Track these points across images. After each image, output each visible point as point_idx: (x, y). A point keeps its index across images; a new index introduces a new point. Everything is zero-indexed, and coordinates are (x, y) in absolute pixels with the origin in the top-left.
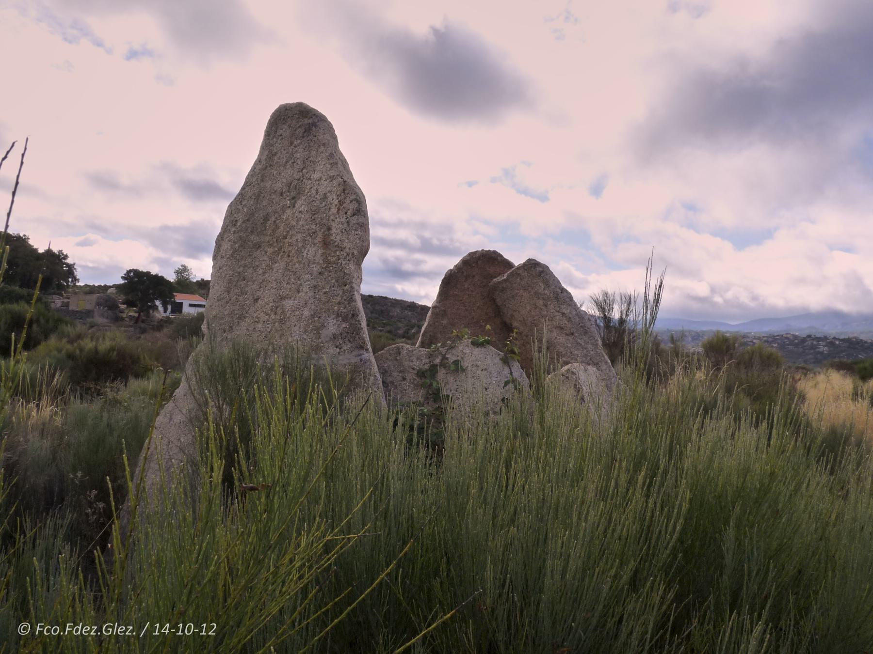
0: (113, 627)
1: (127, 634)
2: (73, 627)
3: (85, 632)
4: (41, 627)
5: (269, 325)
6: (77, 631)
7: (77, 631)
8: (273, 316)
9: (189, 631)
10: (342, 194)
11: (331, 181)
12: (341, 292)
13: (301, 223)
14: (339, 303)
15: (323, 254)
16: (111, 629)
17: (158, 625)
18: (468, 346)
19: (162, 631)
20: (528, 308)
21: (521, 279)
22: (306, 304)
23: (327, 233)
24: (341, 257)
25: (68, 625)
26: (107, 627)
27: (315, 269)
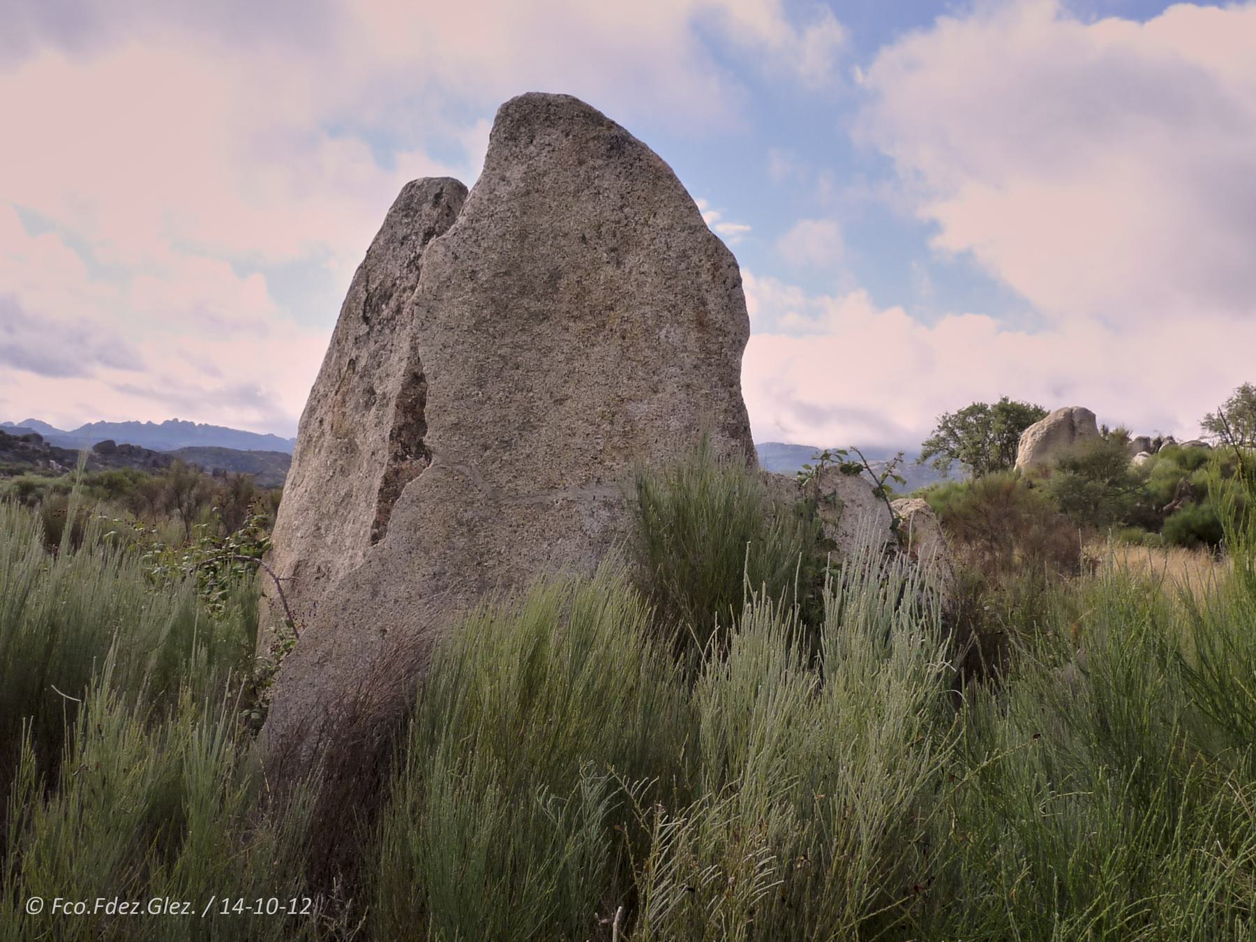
1: (132, 913)
2: (104, 903)
3: (123, 910)
4: (100, 903)
5: (599, 441)
6: (110, 910)
7: (110, 910)
8: (606, 426)
9: (271, 910)
10: (715, 254)
11: (693, 233)
12: (726, 395)
13: (647, 289)
14: (726, 411)
15: (698, 339)
16: (160, 907)
17: (227, 900)
18: (837, 474)
19: (233, 909)
22: (673, 410)
23: (702, 308)
24: (725, 344)
25: (98, 899)
27: (688, 361)
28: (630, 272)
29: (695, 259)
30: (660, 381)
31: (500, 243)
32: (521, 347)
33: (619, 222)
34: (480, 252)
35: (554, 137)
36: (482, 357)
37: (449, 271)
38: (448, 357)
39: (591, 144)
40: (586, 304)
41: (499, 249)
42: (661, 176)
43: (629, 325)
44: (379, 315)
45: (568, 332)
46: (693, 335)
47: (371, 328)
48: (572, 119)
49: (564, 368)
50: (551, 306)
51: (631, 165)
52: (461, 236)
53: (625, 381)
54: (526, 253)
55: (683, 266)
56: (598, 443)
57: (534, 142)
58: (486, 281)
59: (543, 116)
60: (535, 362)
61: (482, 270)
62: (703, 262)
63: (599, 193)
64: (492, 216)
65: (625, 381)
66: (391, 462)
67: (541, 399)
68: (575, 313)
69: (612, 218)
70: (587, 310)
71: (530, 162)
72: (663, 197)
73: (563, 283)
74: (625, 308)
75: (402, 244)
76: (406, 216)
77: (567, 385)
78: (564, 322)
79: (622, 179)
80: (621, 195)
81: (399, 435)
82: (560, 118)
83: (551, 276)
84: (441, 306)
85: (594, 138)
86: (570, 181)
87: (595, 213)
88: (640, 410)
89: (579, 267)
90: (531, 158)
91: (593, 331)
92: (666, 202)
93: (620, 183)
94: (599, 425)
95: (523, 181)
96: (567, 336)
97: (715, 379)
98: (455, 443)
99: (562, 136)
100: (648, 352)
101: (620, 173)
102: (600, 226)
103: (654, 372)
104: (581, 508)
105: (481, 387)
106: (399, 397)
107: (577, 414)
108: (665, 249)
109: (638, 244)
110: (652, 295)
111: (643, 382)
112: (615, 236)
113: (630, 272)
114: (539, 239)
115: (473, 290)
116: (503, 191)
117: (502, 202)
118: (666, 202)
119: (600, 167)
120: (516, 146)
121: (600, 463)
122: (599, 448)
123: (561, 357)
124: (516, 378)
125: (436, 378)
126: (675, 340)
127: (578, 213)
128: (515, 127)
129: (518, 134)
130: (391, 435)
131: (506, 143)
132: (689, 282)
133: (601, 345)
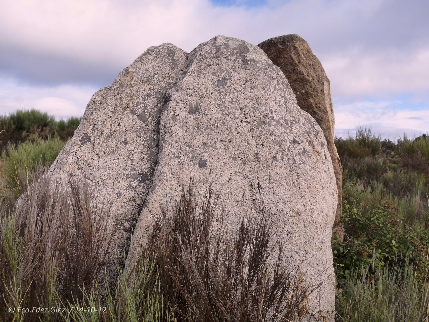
16: (54, 310)
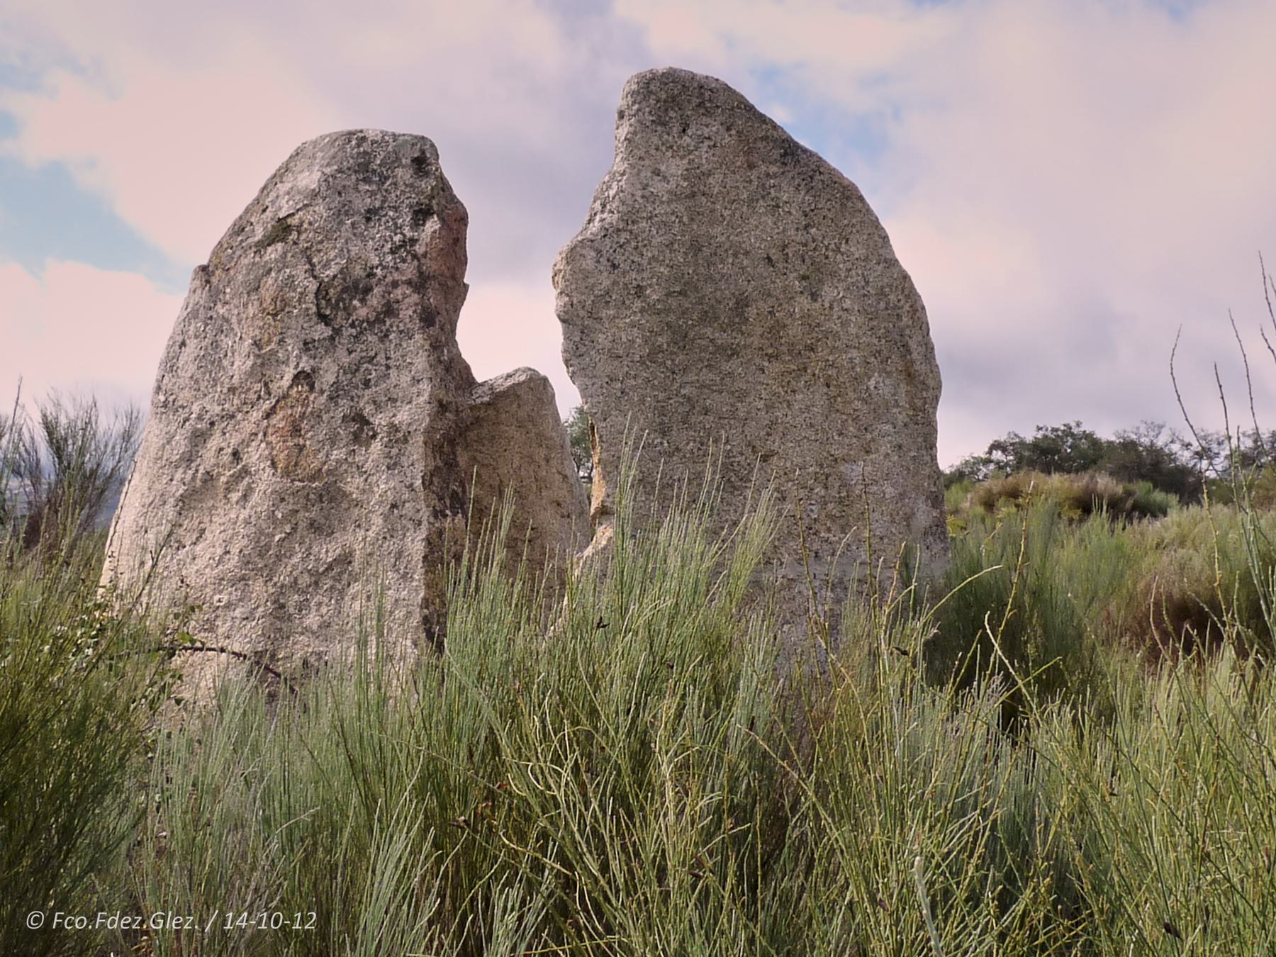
0: (164, 918)
2: (106, 918)
4: (59, 917)
5: (813, 508)
8: (819, 490)
20: (516, 463)
21: (519, 406)
26: (154, 922)
28: (831, 308)
29: (892, 297)
30: (873, 440)
31: (668, 255)
32: (708, 387)
33: (805, 245)
34: (645, 262)
35: (714, 129)
36: (661, 396)
37: (607, 283)
38: (619, 394)
39: (759, 144)
40: (783, 341)
41: (667, 262)
42: (848, 196)
43: (835, 371)
44: (350, 315)
45: (764, 372)
46: (903, 388)
47: (337, 332)
48: (733, 109)
49: (765, 418)
50: (740, 339)
51: (811, 178)
52: (616, 239)
53: (836, 438)
54: (702, 270)
55: (882, 305)
56: (812, 511)
57: (689, 132)
58: (658, 300)
59: (695, 101)
60: (729, 408)
61: (650, 285)
62: (902, 302)
63: (778, 207)
64: (650, 218)
65: (836, 438)
66: (432, 520)
67: (742, 454)
68: (770, 351)
69: (798, 239)
70: (784, 349)
71: (691, 157)
72: (854, 221)
73: (752, 312)
74: (828, 350)
75: (368, 220)
76: (365, 180)
77: (771, 438)
78: (758, 361)
79: (803, 193)
80: (804, 212)
81: (431, 482)
82: (718, 107)
83: (737, 303)
84: (598, 326)
85: (762, 139)
86: (741, 187)
87: (776, 231)
88: (854, 472)
89: (769, 295)
90: (690, 152)
91: (793, 375)
92: (858, 227)
93: (801, 196)
94: (812, 489)
95: (685, 180)
96: (762, 378)
97: (920, 440)
98: (642, 504)
99: (722, 129)
100: (858, 404)
101: (799, 185)
102: (785, 247)
103: (866, 429)
104: (802, 588)
105: (664, 434)
106: (426, 432)
107: (785, 474)
108: (863, 283)
109: (833, 274)
110: (857, 337)
111: (855, 440)
112: (804, 261)
113: (831, 308)
114: (716, 254)
115: (642, 311)
116: (658, 187)
117: (662, 202)
118: (858, 227)
119: (775, 176)
120: (668, 134)
121: (815, 534)
122: (814, 516)
123: (761, 404)
124: (708, 426)
125: (605, 420)
126: (886, 391)
127: (757, 227)
128: (662, 108)
129: (667, 119)
130: (423, 483)
131: (654, 127)
132: (891, 325)
133: (802, 392)
